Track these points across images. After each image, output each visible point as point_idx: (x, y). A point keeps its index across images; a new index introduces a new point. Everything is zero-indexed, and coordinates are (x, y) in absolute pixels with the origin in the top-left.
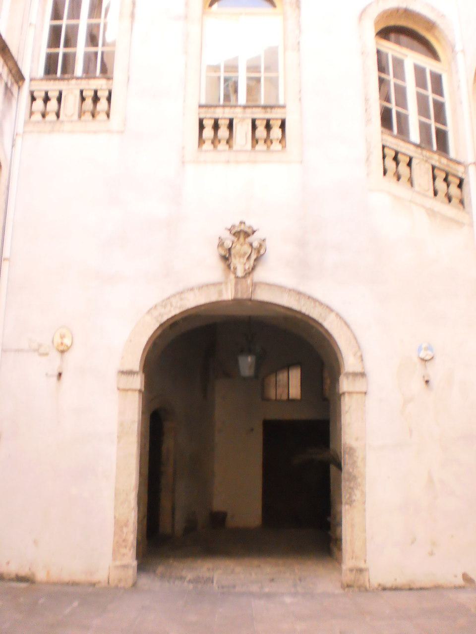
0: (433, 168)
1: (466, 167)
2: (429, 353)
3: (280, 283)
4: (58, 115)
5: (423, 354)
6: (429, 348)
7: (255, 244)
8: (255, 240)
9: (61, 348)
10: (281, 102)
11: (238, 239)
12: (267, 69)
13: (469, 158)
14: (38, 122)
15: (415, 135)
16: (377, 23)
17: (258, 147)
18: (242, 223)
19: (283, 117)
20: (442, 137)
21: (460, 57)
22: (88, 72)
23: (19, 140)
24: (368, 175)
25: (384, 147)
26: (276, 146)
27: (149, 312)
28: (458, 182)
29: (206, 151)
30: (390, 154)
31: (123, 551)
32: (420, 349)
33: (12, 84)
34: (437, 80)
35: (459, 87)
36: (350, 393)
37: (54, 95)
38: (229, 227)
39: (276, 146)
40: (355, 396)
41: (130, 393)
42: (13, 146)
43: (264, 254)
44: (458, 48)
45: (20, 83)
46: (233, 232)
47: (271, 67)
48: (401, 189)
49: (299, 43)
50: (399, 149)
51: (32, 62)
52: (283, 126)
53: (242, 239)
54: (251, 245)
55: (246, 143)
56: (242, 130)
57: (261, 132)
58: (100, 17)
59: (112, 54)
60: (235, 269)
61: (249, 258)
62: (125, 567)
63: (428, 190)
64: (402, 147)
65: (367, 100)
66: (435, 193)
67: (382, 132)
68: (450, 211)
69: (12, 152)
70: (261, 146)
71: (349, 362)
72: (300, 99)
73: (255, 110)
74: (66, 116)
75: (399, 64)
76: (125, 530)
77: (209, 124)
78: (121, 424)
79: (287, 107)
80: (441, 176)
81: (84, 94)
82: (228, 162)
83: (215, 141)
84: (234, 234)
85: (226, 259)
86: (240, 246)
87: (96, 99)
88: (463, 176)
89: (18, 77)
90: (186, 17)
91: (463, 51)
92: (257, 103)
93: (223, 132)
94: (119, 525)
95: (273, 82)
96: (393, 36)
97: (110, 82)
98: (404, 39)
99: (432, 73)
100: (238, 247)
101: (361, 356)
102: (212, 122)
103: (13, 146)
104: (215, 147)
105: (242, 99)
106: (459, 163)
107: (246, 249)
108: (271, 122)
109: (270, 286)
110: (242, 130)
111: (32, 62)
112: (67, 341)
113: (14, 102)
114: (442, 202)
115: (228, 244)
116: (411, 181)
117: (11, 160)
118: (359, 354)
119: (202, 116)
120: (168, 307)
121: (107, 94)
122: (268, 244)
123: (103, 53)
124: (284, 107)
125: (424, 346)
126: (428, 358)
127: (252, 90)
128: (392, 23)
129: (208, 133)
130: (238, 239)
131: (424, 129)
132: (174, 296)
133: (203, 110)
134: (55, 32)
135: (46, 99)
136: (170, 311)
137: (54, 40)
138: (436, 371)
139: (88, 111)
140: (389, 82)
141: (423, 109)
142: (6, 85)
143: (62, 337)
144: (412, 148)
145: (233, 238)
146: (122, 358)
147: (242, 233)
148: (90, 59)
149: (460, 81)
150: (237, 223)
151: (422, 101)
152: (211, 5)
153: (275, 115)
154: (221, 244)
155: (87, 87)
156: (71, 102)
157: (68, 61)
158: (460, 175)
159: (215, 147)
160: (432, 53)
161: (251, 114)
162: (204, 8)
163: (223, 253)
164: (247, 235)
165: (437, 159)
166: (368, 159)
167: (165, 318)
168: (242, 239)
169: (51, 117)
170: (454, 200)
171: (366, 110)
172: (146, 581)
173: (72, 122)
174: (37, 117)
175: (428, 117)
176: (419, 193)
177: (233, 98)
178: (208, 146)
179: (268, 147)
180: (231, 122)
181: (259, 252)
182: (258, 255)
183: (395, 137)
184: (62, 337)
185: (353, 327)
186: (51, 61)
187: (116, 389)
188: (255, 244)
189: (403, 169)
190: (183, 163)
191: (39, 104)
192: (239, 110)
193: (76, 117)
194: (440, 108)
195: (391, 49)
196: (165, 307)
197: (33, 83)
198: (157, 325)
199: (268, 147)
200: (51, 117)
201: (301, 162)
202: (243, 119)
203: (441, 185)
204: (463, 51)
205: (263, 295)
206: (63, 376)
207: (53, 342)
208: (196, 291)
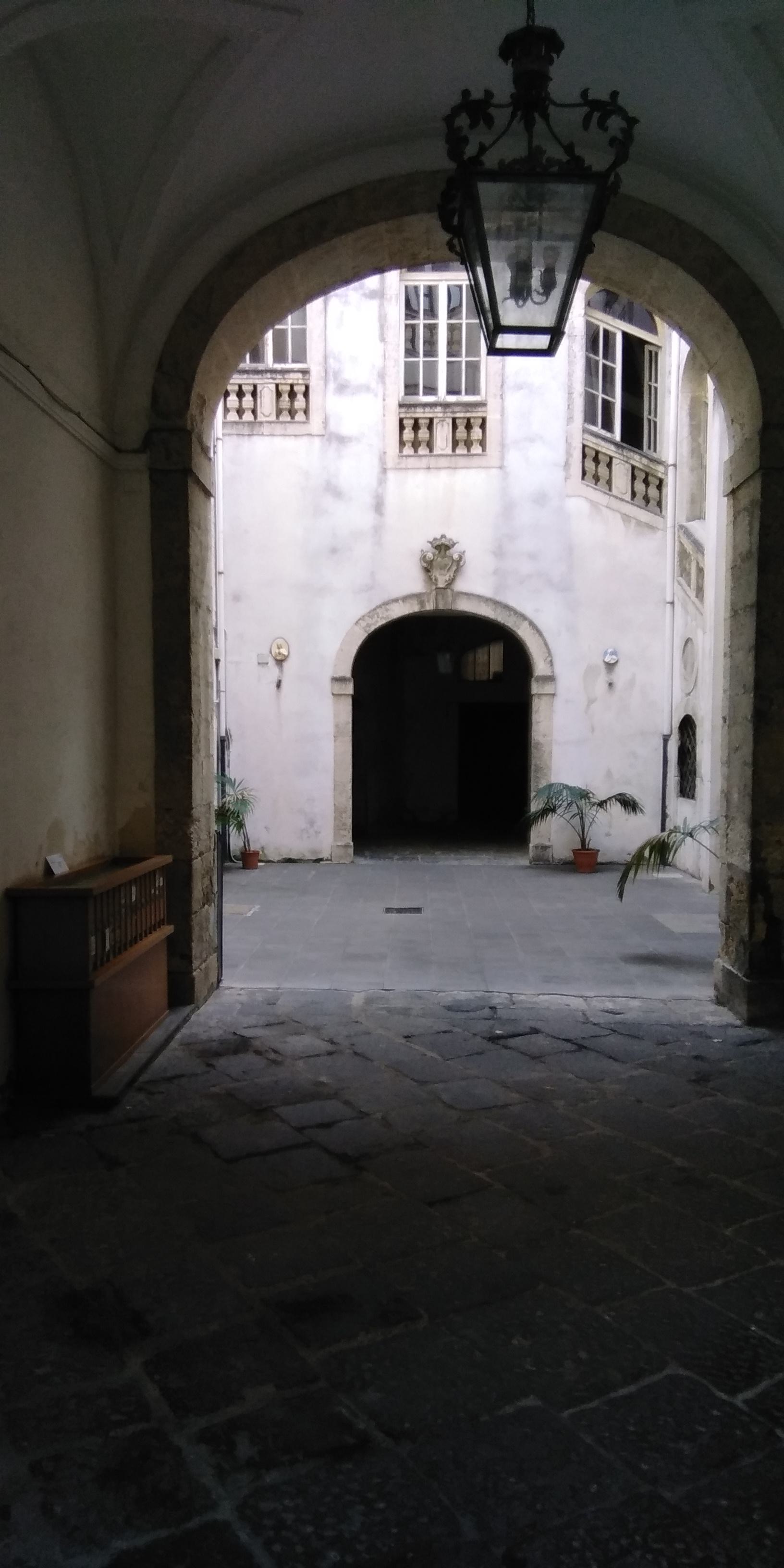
0: (633, 468)
1: (666, 467)
2: (614, 657)
3: (478, 588)
4: (254, 412)
5: (608, 659)
6: (614, 653)
7: (456, 557)
8: (455, 553)
9: (279, 658)
17: (459, 451)
18: (443, 536)
19: (484, 415)
24: (566, 479)
25: (584, 446)
27: (357, 623)
28: (657, 483)
29: (407, 456)
30: (591, 454)
31: (343, 833)
32: (606, 653)
36: (540, 695)
37: (247, 389)
39: (476, 449)
40: (544, 698)
41: (343, 698)
50: (600, 449)
52: (483, 426)
56: (443, 434)
60: (436, 580)
62: (346, 846)
65: (570, 394)
68: (644, 516)
70: (461, 450)
71: (540, 668)
76: (344, 815)
77: (408, 423)
78: (337, 726)
80: (641, 476)
81: (280, 388)
83: (416, 444)
84: (436, 548)
85: (427, 570)
86: (441, 557)
87: (292, 394)
88: (663, 477)
91: (675, 465)
94: (338, 811)
100: (439, 559)
101: (551, 661)
102: (412, 422)
108: (472, 421)
109: (469, 595)
112: (284, 651)
116: (609, 483)
118: (549, 659)
119: (402, 416)
120: (375, 618)
121: (303, 388)
125: (610, 651)
126: (612, 662)
132: (380, 606)
133: (403, 410)
136: (377, 622)
138: (621, 675)
143: (279, 647)
144: (612, 447)
146: (335, 665)
147: (442, 547)
150: (439, 537)
154: (424, 558)
155: (283, 381)
158: (660, 475)
163: (425, 565)
164: (448, 548)
167: (373, 628)
172: (370, 867)
176: (616, 497)
178: (408, 450)
180: (431, 420)
182: (458, 565)
184: (279, 647)
185: (545, 634)
187: (331, 695)
188: (456, 557)
189: (603, 470)
196: (371, 617)
198: (366, 635)
201: (501, 467)
202: (442, 420)
203: (640, 487)
204: (675, 465)
205: (465, 606)
206: (283, 684)
207: (271, 652)
208: (400, 602)
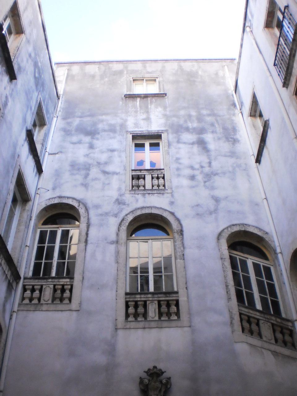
7: (164, 381)
8: (163, 378)
10: (176, 289)
11: (152, 379)
12: (165, 268)
13: (295, 317)
14: (27, 304)
15: (259, 306)
16: (228, 241)
20: (276, 305)
21: (280, 256)
22: (59, 274)
23: (15, 315)
26: (174, 317)
33: (13, 281)
34: (268, 270)
35: (282, 274)
38: (146, 370)
42: (11, 319)
43: (170, 387)
44: (278, 250)
45: (18, 281)
46: (149, 374)
47: (168, 267)
48: (255, 341)
49: (183, 255)
51: (26, 268)
53: (155, 378)
54: (161, 382)
55: (155, 316)
56: (152, 310)
57: (164, 309)
58: (67, 243)
59: (74, 264)
61: (160, 391)
63: (272, 339)
64: (252, 313)
65: (227, 286)
66: (276, 341)
67: (238, 305)
69: (10, 322)
72: (186, 288)
73: (159, 296)
74: (44, 300)
75: (244, 264)
79: (179, 292)
82: (144, 328)
89: (16, 276)
90: (117, 242)
92: (161, 291)
93: (141, 310)
95: (170, 278)
96: (238, 247)
97: (72, 281)
98: (245, 248)
99: (263, 266)
100: (153, 383)
103: (11, 319)
104: (136, 319)
105: (152, 288)
106: (288, 320)
107: (158, 384)
110: (152, 310)
111: (26, 268)
113: (13, 293)
114: (281, 346)
115: (146, 381)
117: (9, 326)
122: (173, 381)
123: (68, 262)
124: (177, 293)
127: (157, 281)
128: (237, 240)
129: (131, 310)
130: (152, 379)
131: (264, 301)
134: (40, 250)
135: (33, 290)
137: (39, 256)
139: (58, 298)
140: (239, 274)
141: (261, 289)
142: (9, 281)
144: (258, 314)
145: (149, 378)
148: (60, 266)
149: (282, 271)
150: (152, 368)
151: (260, 284)
152: (131, 235)
153: (173, 297)
156: (48, 293)
157: (48, 267)
159: (136, 319)
160: (265, 257)
161: (156, 297)
162: (127, 236)
163: (143, 388)
165: (274, 320)
166: (231, 323)
168: (155, 378)
169: (35, 301)
170: (289, 344)
171: (227, 292)
173: (48, 304)
174: (27, 301)
175: (266, 294)
177: (145, 287)
178: (131, 318)
179: (169, 318)
181: (166, 387)
183: (246, 307)
186: (37, 267)
188: (164, 381)
190: (116, 329)
191: (28, 293)
192: (150, 296)
193: (50, 302)
194: (272, 287)
195: (239, 255)
197: (26, 281)
199: (169, 318)
200: (35, 301)
202: (152, 301)
